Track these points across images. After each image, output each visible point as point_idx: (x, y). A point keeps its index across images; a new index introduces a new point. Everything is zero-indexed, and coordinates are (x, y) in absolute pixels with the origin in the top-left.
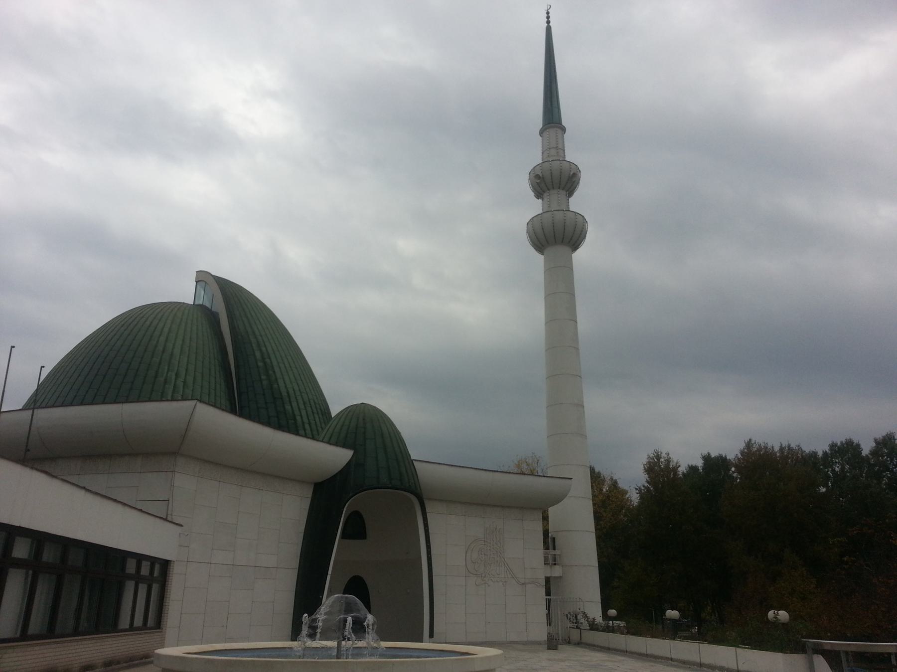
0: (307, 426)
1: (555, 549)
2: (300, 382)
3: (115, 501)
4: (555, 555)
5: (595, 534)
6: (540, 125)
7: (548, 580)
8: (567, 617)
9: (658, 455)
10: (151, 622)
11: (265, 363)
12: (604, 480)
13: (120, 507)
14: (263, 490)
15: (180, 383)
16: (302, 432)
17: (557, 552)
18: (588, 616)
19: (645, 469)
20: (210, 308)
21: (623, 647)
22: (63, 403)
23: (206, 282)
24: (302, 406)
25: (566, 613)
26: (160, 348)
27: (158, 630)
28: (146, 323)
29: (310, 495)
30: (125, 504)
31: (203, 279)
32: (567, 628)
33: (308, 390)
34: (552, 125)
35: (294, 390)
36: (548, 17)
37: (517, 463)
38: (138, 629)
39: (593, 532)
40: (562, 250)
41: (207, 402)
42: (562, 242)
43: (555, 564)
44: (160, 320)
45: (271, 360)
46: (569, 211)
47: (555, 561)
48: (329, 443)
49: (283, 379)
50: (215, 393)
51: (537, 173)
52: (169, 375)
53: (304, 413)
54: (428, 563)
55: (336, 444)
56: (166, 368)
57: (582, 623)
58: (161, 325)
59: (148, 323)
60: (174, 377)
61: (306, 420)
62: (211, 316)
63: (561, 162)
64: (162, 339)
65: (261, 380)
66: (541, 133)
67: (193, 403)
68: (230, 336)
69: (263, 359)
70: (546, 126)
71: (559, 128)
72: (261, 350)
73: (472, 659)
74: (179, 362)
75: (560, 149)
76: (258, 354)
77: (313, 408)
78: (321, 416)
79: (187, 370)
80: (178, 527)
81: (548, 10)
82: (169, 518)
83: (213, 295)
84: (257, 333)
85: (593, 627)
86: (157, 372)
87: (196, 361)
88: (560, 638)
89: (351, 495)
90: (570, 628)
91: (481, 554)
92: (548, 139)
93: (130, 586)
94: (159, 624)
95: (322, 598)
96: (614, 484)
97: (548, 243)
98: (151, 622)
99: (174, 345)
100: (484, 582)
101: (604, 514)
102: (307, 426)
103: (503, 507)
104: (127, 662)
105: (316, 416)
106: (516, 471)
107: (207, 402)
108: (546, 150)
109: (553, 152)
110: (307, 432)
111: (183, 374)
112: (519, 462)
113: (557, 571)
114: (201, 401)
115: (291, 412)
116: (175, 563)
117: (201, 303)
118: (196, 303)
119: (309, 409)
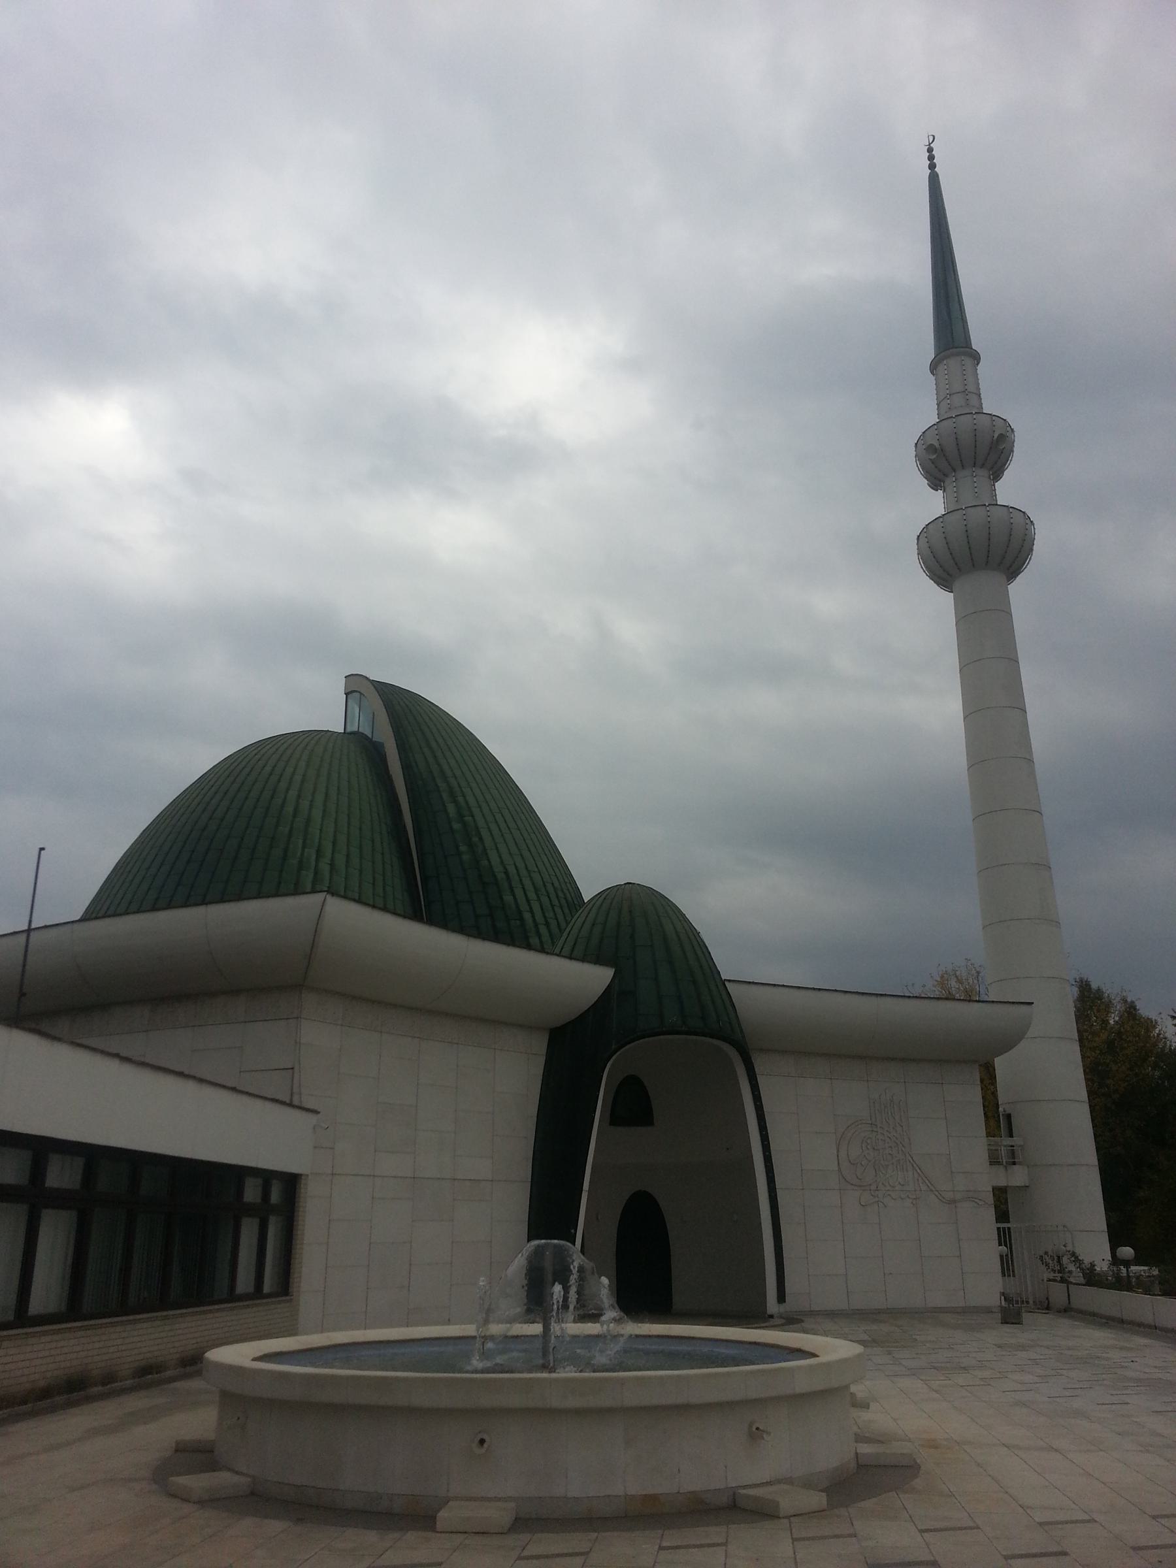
1: (1011, 1136)
2: (526, 854)
6: (930, 354)
7: (1001, 1196)
8: (1042, 1261)
12: (1108, 1005)
13: (191, 1085)
14: (457, 1044)
15: (325, 867)
16: (534, 941)
17: (1016, 1140)
18: (1080, 1258)
20: (370, 736)
21: (1149, 1319)
22: (139, 909)
24: (532, 895)
25: (1042, 1253)
26: (290, 809)
27: (284, 1298)
29: (544, 1052)
30: (201, 1081)
32: (1043, 1280)
34: (954, 350)
35: (516, 867)
36: (931, 158)
37: (939, 979)
41: (342, 894)
43: (1014, 1163)
46: (997, 505)
47: (1014, 1158)
48: (571, 958)
49: (497, 849)
51: (928, 444)
52: (305, 854)
54: (766, 1166)
55: (583, 959)
56: (301, 841)
57: (1070, 1272)
58: (290, 770)
59: (268, 769)
60: (314, 857)
62: (371, 750)
63: (975, 416)
64: (293, 794)
66: (934, 367)
67: (321, 896)
69: (461, 816)
70: (942, 354)
71: (965, 354)
72: (455, 802)
75: (971, 393)
76: (451, 808)
77: (553, 896)
79: (334, 843)
80: (310, 1115)
82: (296, 1102)
83: (374, 713)
84: (449, 773)
85: (1092, 1278)
86: (286, 851)
87: (348, 828)
90: (1050, 1280)
91: (868, 1149)
94: (285, 1287)
95: (576, 1233)
96: (1131, 1010)
100: (877, 1199)
101: (1114, 1068)
102: (543, 930)
103: (903, 1060)
105: (558, 910)
106: (937, 995)
107: (357, 898)
108: (944, 399)
109: (958, 400)
112: (942, 977)
113: (1017, 1177)
114: (333, 893)
116: (310, 1177)
117: (357, 730)
118: (349, 730)
119: (545, 900)
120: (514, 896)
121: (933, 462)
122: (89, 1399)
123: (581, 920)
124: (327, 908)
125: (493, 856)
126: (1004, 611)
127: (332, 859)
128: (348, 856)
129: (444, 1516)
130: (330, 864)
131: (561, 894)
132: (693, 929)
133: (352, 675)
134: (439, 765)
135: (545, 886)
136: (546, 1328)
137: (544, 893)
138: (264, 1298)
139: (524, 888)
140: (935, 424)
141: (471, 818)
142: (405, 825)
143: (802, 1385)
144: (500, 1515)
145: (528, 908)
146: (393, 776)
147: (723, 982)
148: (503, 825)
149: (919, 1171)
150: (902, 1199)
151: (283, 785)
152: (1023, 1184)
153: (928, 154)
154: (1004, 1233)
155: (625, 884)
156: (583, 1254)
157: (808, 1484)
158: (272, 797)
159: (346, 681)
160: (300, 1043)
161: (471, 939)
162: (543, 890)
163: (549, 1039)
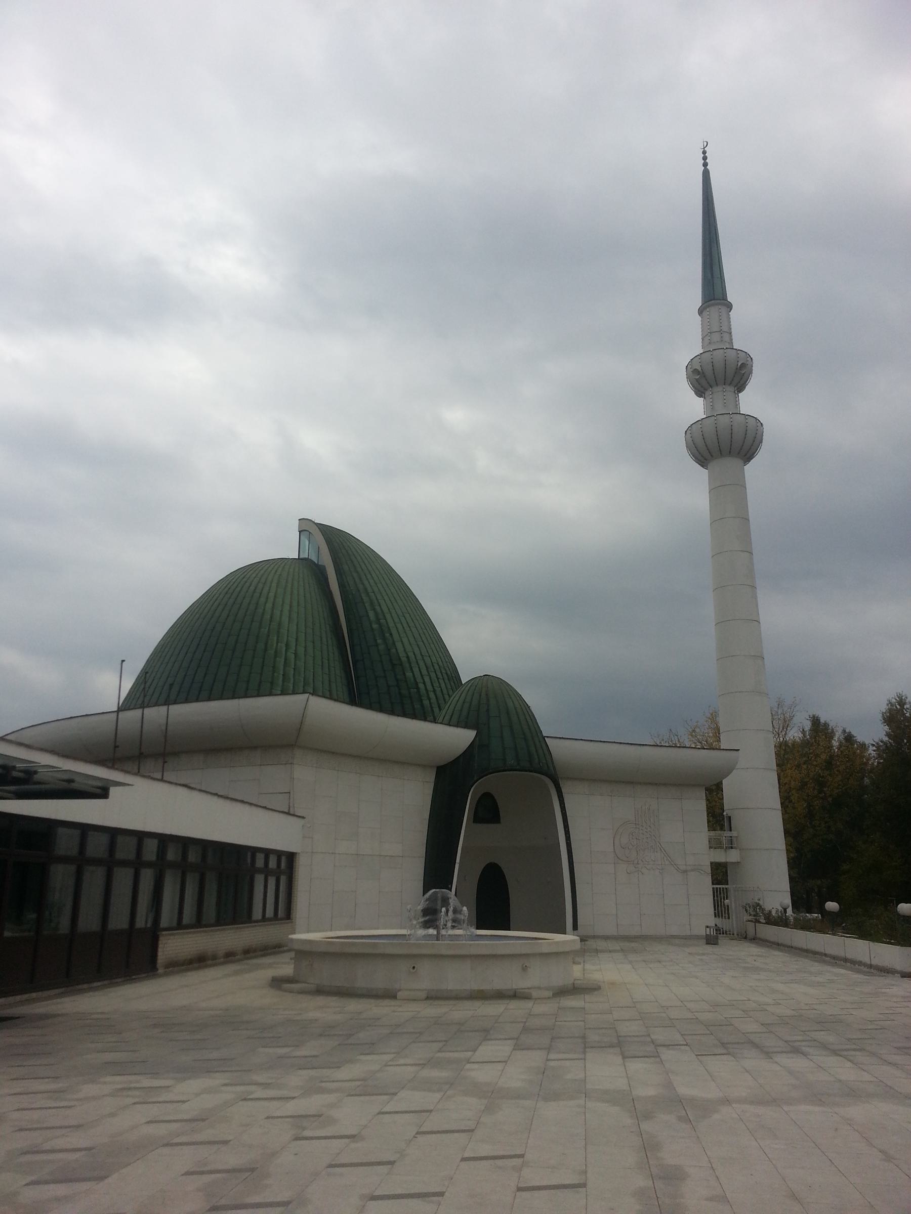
0: (432, 695)
1: (731, 831)
2: (421, 644)
3: (242, 802)
4: (731, 837)
5: (781, 812)
6: (699, 303)
9: (901, 699)
10: (281, 913)
11: (380, 625)
12: (830, 735)
13: (247, 807)
14: (382, 777)
15: (292, 656)
19: (884, 719)
20: (316, 562)
23: (310, 533)
24: (424, 672)
26: (267, 616)
28: (251, 588)
30: (251, 804)
31: (307, 528)
33: (430, 651)
36: (705, 158)
38: (270, 920)
39: (778, 810)
40: (730, 464)
42: (730, 453)
43: (732, 848)
44: (265, 583)
45: (386, 621)
47: (732, 845)
50: (329, 663)
51: (694, 368)
53: (427, 679)
55: (457, 726)
56: (275, 638)
59: (252, 588)
60: (284, 649)
61: (429, 687)
62: (318, 572)
64: (269, 605)
65: (377, 645)
66: (701, 312)
68: (340, 599)
69: (378, 620)
72: (374, 610)
73: (541, 943)
74: (288, 630)
75: (725, 332)
76: (371, 614)
78: (447, 681)
79: (297, 640)
81: (704, 148)
82: (292, 812)
84: (369, 589)
86: (266, 644)
88: (735, 933)
89: (475, 779)
91: (633, 839)
92: (708, 317)
93: (259, 879)
94: (288, 915)
96: (849, 738)
97: (712, 456)
98: (281, 913)
99: (282, 611)
100: (637, 869)
101: (830, 779)
102: (432, 695)
104: (263, 951)
105: (441, 681)
108: (707, 335)
110: (432, 701)
111: (293, 644)
113: (733, 856)
114: (314, 693)
115: (412, 679)
117: (307, 557)
119: (433, 675)
120: (413, 672)
121: (697, 380)
122: (206, 966)
123: (457, 698)
124: (310, 701)
125: (399, 645)
126: (741, 485)
127: (296, 650)
128: (305, 647)
129: (399, 994)
130: (294, 653)
131: (443, 671)
132: (525, 704)
133: (303, 519)
134: (363, 584)
135: (433, 666)
136: (438, 933)
137: (433, 670)
138: (278, 920)
139: (419, 667)
140: (698, 355)
141: (385, 621)
142: (341, 625)
143: (545, 950)
144: (423, 995)
145: (422, 681)
146: (333, 591)
147: (544, 737)
148: (405, 625)
149: (664, 852)
150: (653, 869)
151: (263, 600)
152: (736, 861)
153: (703, 161)
154: (717, 892)
155: (484, 675)
156: (456, 897)
157: (547, 989)
158: (256, 609)
159: (299, 522)
160: (293, 778)
161: (390, 716)
162: (432, 668)
163: (437, 772)
